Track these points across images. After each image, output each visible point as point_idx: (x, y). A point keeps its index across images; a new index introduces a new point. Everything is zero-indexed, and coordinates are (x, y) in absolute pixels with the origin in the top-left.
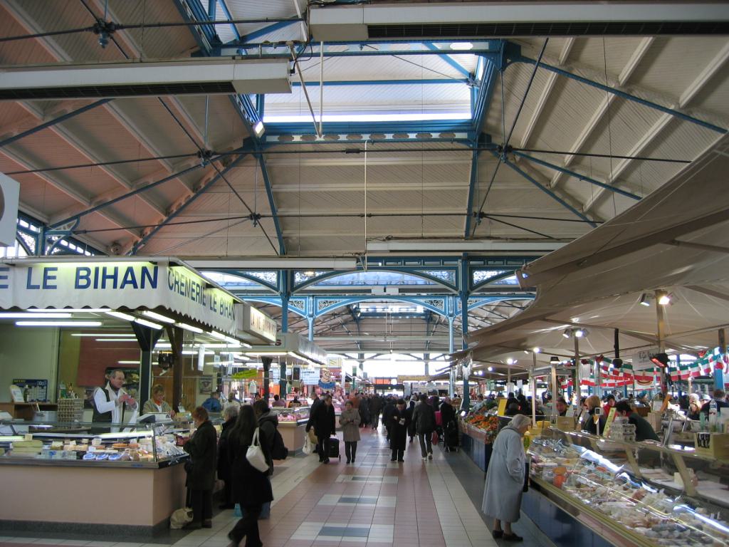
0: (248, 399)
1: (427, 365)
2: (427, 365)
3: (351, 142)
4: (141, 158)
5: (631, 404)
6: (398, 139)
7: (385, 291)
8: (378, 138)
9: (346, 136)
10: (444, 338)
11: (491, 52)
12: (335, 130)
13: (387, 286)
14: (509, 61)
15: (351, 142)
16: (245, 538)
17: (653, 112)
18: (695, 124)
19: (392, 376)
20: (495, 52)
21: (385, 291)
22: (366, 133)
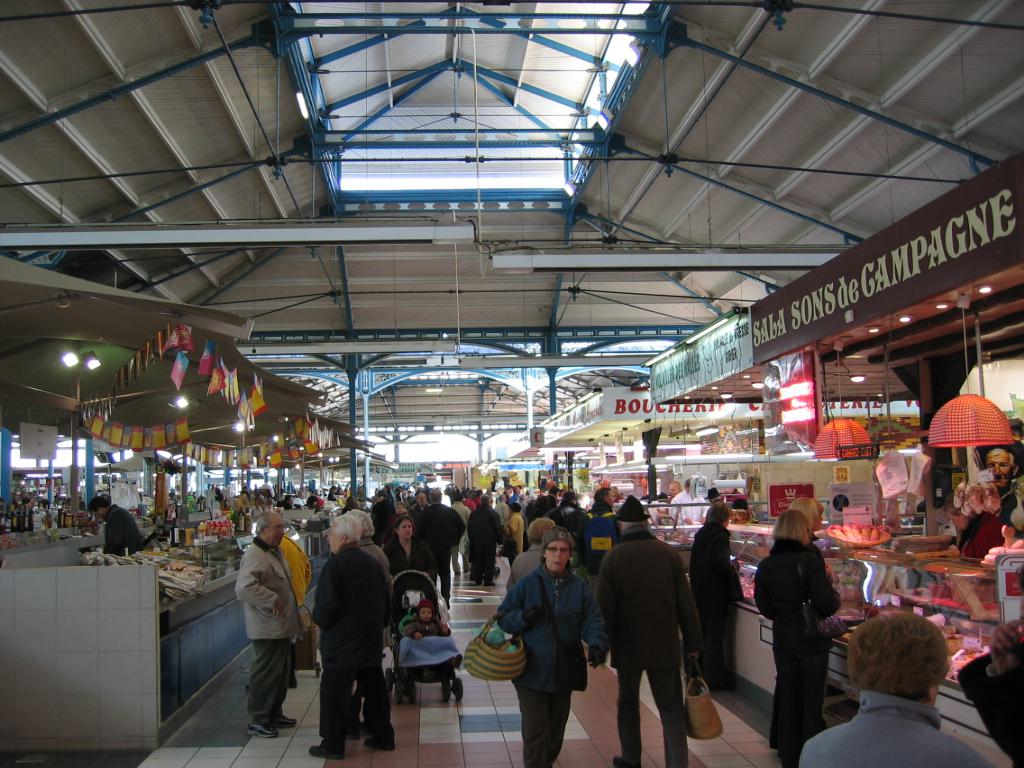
0: (827, 630)
1: (396, 447)
2: (396, 447)
3: (414, 211)
4: (65, 178)
5: (137, 436)
6: (412, 209)
7: (442, 362)
8: (417, 208)
9: (432, 204)
10: (371, 413)
11: (648, 33)
12: (420, 199)
13: (445, 357)
14: (671, 45)
15: (414, 211)
16: (645, 677)
17: (829, 105)
18: (762, 75)
19: (436, 461)
20: (655, 33)
21: (442, 362)
22: (454, 201)
